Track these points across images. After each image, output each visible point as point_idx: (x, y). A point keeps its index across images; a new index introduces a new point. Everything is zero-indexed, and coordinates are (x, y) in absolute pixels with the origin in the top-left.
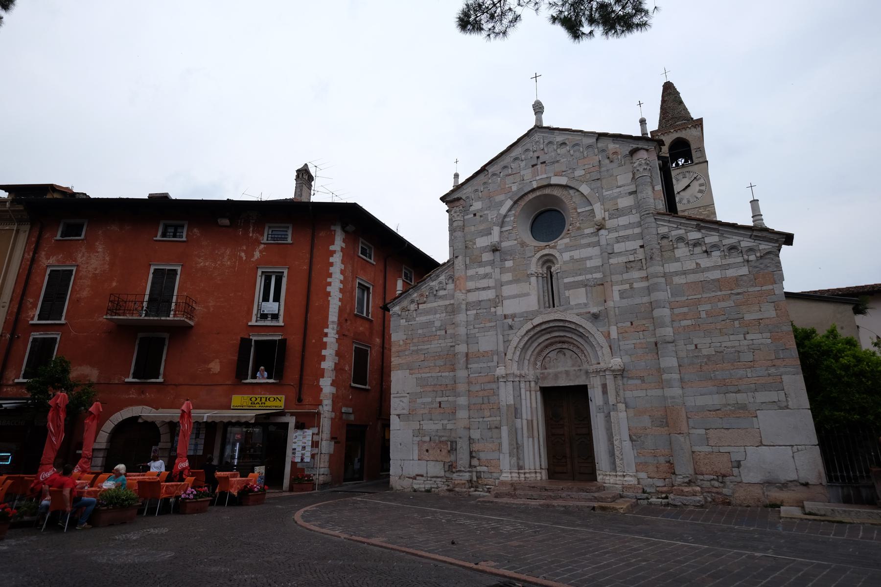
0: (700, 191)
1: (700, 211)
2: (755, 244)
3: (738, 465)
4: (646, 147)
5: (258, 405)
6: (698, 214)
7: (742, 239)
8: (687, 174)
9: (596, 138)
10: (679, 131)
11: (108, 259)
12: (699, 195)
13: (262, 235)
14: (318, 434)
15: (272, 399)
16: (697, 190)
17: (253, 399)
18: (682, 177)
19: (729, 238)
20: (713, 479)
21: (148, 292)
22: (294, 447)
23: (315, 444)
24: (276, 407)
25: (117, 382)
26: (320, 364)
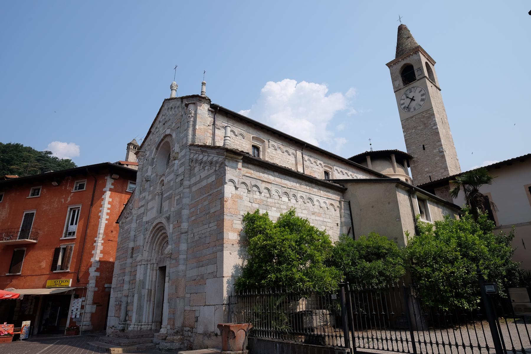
0: (423, 100)
1: (423, 115)
4: (193, 102)
5: (58, 285)
6: (422, 117)
8: (413, 89)
9: (180, 101)
10: (405, 59)
11: (8, 211)
12: (422, 103)
13: (73, 188)
14: (84, 301)
15: (64, 281)
16: (420, 99)
17: (56, 282)
18: (409, 92)
21: (21, 226)
22: (72, 309)
23: (83, 307)
24: (66, 286)
25: (3, 275)
26: (90, 259)
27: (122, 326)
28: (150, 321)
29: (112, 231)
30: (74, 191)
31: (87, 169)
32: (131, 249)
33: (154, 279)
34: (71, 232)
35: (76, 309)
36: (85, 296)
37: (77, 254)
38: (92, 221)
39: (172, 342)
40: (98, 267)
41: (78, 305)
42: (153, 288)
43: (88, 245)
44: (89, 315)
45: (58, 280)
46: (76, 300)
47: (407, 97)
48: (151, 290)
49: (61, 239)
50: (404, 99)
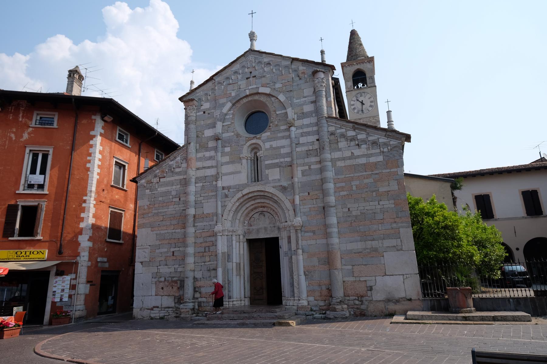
0: (371, 106)
1: (370, 119)
2: (388, 141)
3: (371, 288)
4: (323, 70)
5: (23, 258)
7: (380, 137)
8: (363, 94)
9: (290, 61)
12: (370, 109)
13: (31, 120)
15: (36, 253)
16: (369, 105)
19: (372, 136)
20: (355, 299)
22: (54, 290)
23: (73, 287)
24: (39, 258)
26: (79, 224)
27: (193, 304)
28: (243, 296)
29: (103, 190)
30: (33, 125)
31: (73, 100)
32: (192, 216)
33: (242, 252)
34: (33, 185)
35: (60, 290)
36: (76, 272)
37: (51, 215)
38: (76, 173)
39: (342, 311)
40: (91, 235)
41: (64, 285)
42: (242, 262)
43: (73, 205)
44: (82, 298)
45: (22, 251)
46: (59, 278)
47: (358, 100)
48: (240, 264)
49: (17, 192)
50: (354, 101)
